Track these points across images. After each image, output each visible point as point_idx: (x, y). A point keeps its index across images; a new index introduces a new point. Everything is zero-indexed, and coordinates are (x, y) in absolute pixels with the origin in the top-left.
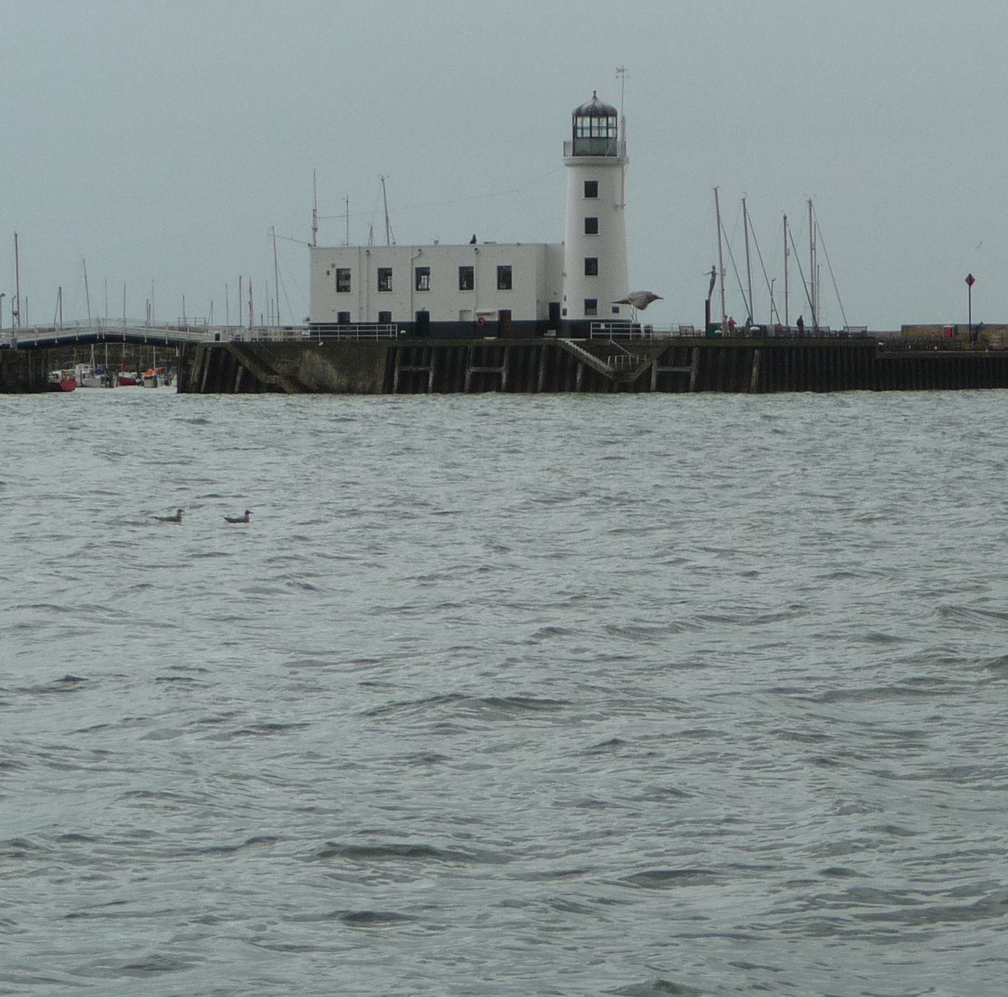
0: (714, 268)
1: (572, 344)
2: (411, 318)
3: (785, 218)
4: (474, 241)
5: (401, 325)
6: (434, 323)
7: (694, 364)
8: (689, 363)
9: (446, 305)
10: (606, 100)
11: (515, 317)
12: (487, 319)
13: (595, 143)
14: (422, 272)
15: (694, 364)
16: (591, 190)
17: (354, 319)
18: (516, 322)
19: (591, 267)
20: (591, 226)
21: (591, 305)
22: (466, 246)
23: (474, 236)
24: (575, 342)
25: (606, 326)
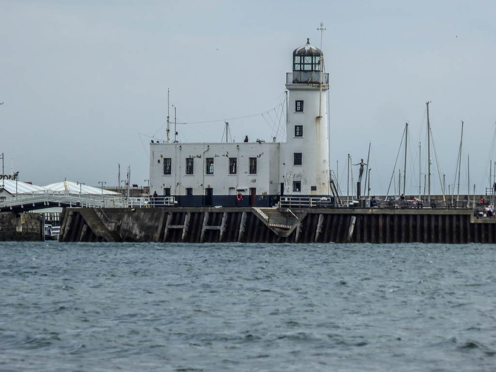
0: (362, 160)
1: (263, 214)
2: (184, 193)
3: (407, 125)
4: (246, 140)
5: (177, 198)
6: (214, 196)
7: (203, 230)
8: (220, 225)
9: (222, 183)
10: (313, 47)
11: (194, 193)
12: (243, 194)
13: (306, 73)
14: (210, 161)
15: (203, 230)
16: (300, 106)
17: (194, 193)
18: (196, 196)
19: (298, 159)
20: (299, 131)
21: (297, 185)
22: (243, 143)
23: (247, 137)
24: (263, 211)
25: (288, 199)
